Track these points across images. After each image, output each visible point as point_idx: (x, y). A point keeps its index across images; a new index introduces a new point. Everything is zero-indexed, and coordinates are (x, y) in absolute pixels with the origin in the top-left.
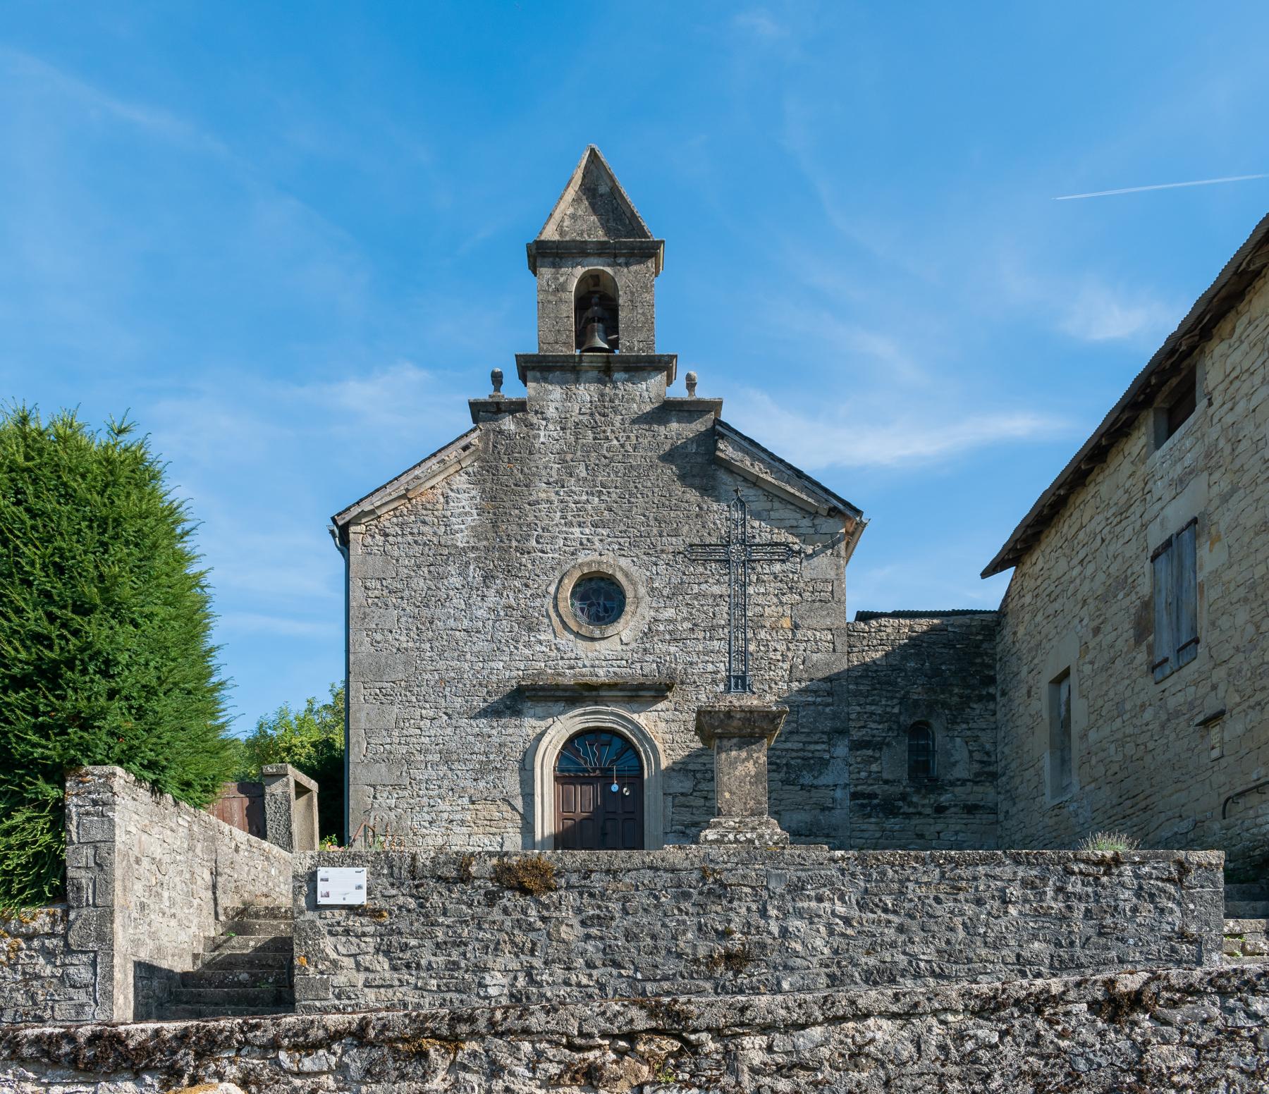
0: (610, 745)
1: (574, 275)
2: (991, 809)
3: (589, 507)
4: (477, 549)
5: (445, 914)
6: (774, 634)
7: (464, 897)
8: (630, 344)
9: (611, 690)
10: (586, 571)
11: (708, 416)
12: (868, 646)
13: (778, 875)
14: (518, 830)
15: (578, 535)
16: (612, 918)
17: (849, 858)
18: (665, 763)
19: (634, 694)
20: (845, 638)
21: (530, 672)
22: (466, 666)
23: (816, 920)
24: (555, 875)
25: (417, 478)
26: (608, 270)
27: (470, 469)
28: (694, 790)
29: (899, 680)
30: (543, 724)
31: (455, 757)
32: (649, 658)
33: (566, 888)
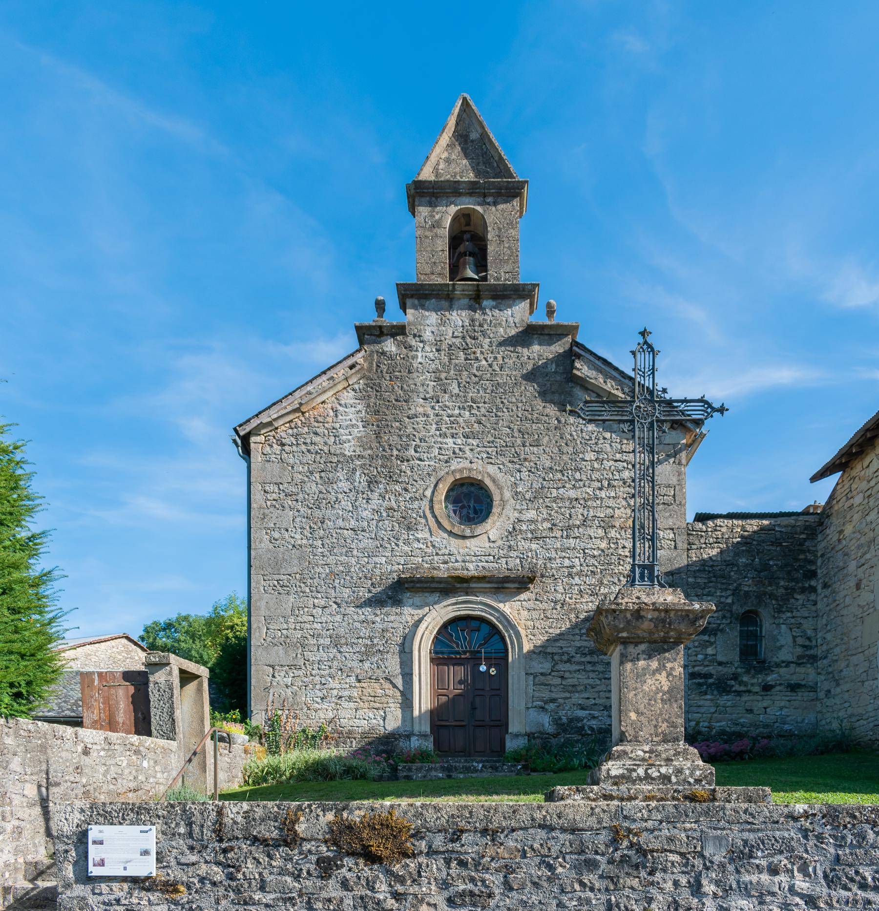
0: (479, 630)
1: (448, 213)
2: (812, 687)
3: (461, 420)
4: (363, 457)
5: (262, 888)
6: (623, 533)
7: (289, 866)
8: (497, 274)
9: (481, 582)
10: (458, 477)
11: (566, 339)
12: (705, 543)
13: (717, 838)
14: (398, 705)
15: (451, 445)
16: (490, 895)
17: (814, 815)
18: (527, 647)
20: (685, 537)
21: (409, 566)
22: (353, 561)
23: (768, 899)
24: (412, 836)
25: (310, 393)
26: (479, 208)
27: (356, 386)
28: (552, 671)
29: (732, 574)
30: (421, 612)
31: (343, 641)
32: (513, 554)
33: (427, 854)
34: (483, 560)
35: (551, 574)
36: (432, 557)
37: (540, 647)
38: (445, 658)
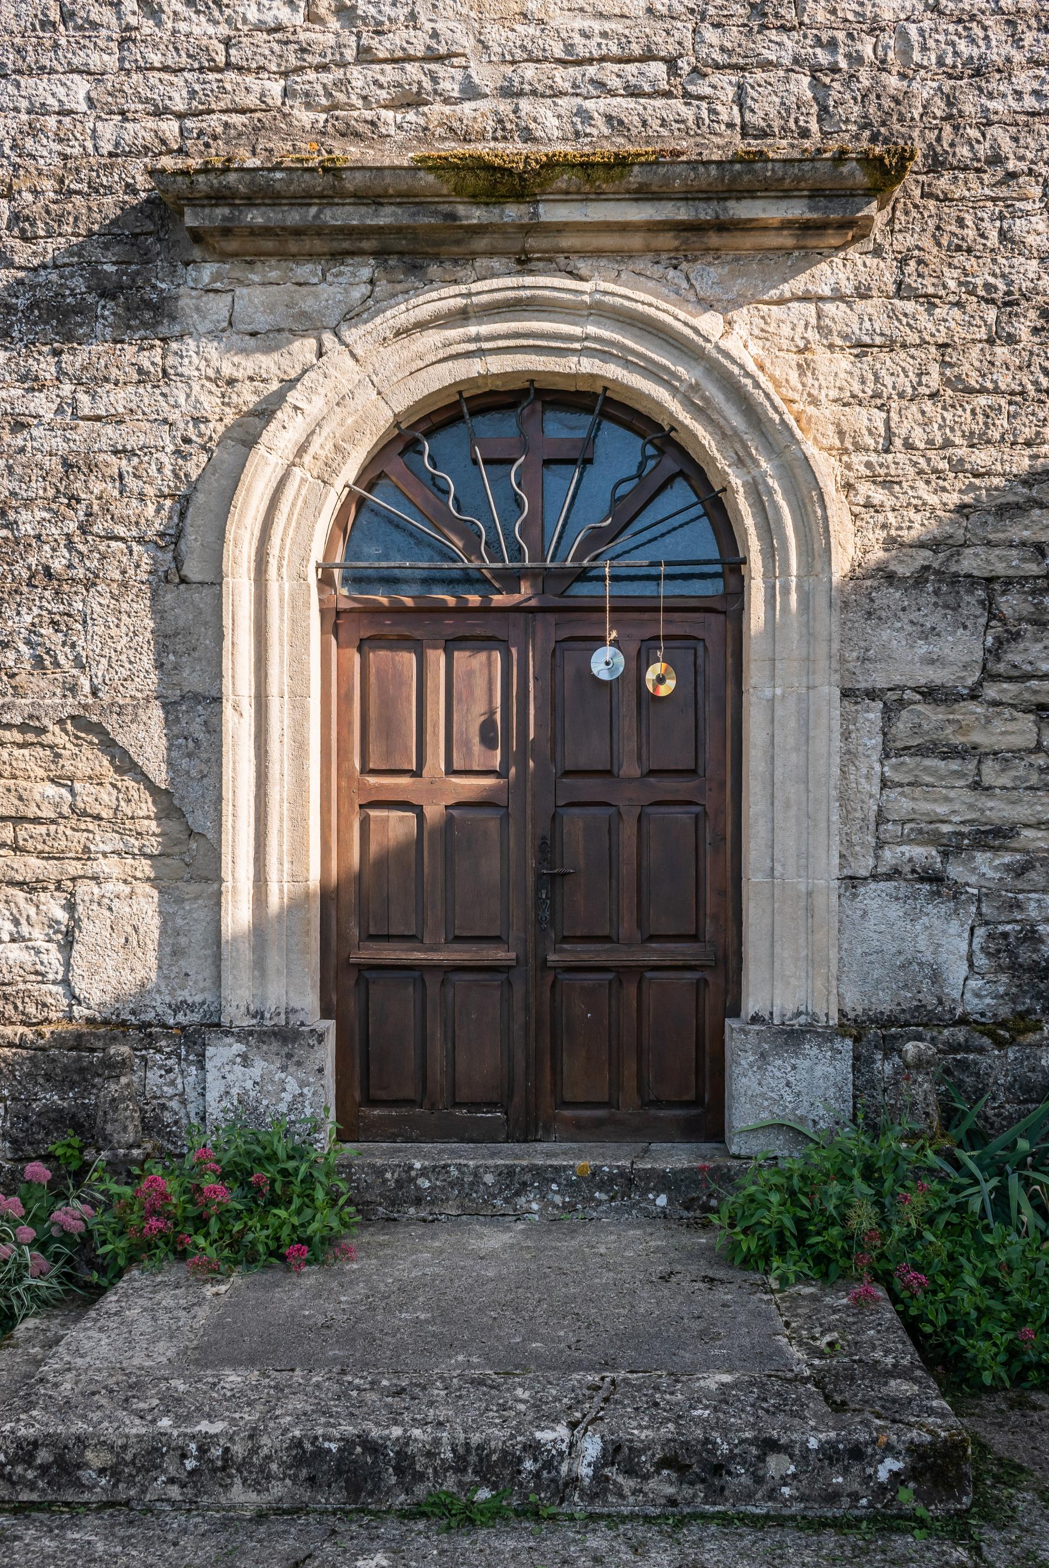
9: (599, 196)
14: (145, 867)
19: (706, 212)
21: (214, 122)
28: (989, 676)
34: (614, 83)
35: (983, 150)
36: (338, 73)
37: (921, 545)
38: (405, 610)
